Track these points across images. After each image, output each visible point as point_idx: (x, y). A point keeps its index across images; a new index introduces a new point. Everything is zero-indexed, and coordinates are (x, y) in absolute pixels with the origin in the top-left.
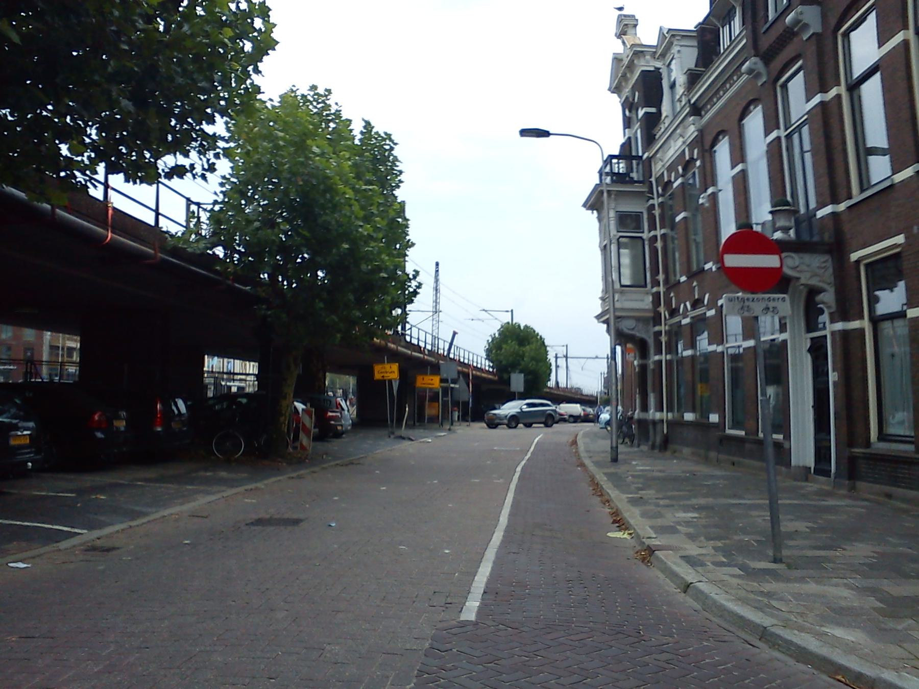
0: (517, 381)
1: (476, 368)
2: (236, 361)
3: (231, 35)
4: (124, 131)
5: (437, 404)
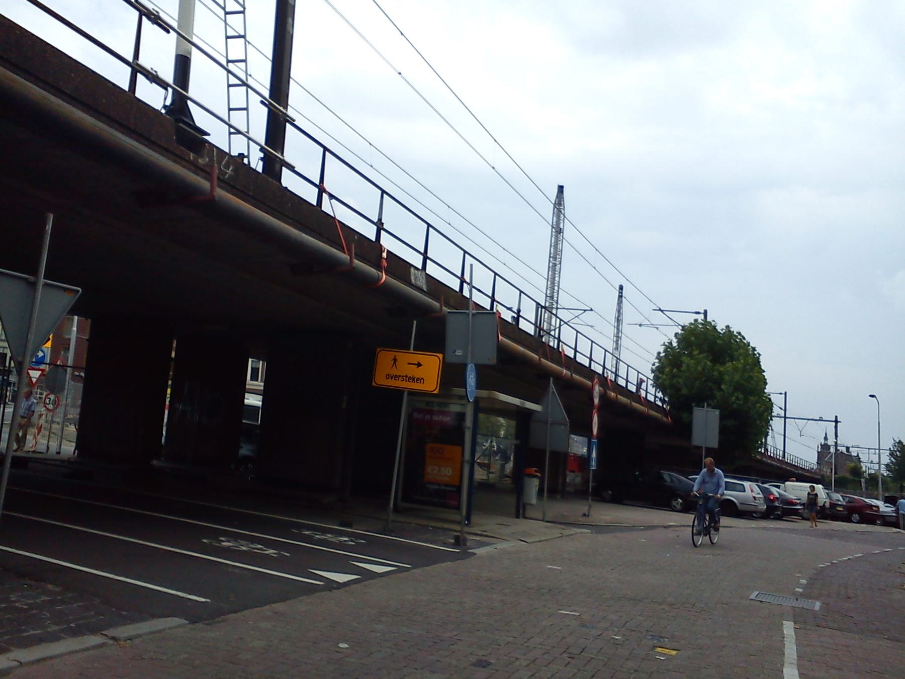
5: (458, 449)
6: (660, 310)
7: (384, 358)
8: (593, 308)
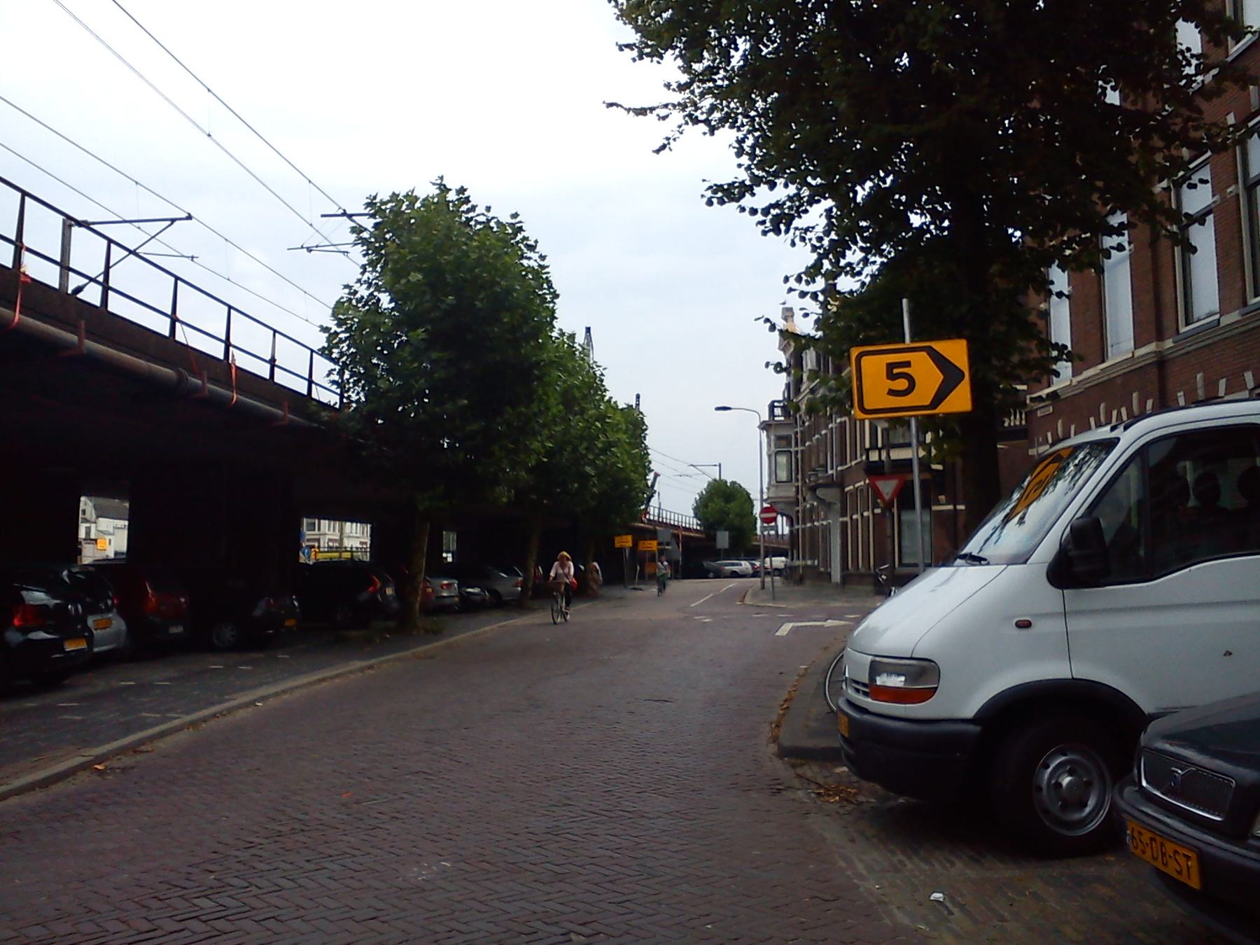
0: (723, 539)
1: (686, 529)
2: (322, 521)
6: (344, 214)
7: (617, 539)
8: (192, 214)
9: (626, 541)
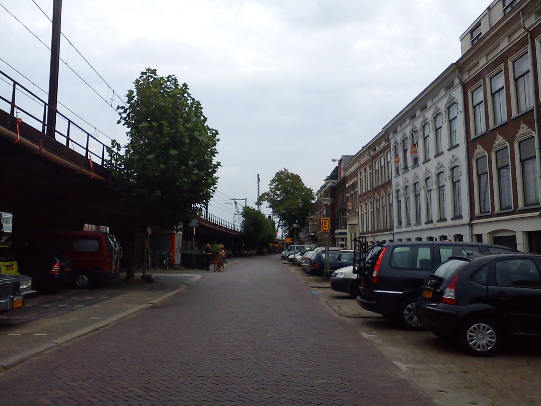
3: (526, 127)
4: (148, 119)
9: (272, 245)
